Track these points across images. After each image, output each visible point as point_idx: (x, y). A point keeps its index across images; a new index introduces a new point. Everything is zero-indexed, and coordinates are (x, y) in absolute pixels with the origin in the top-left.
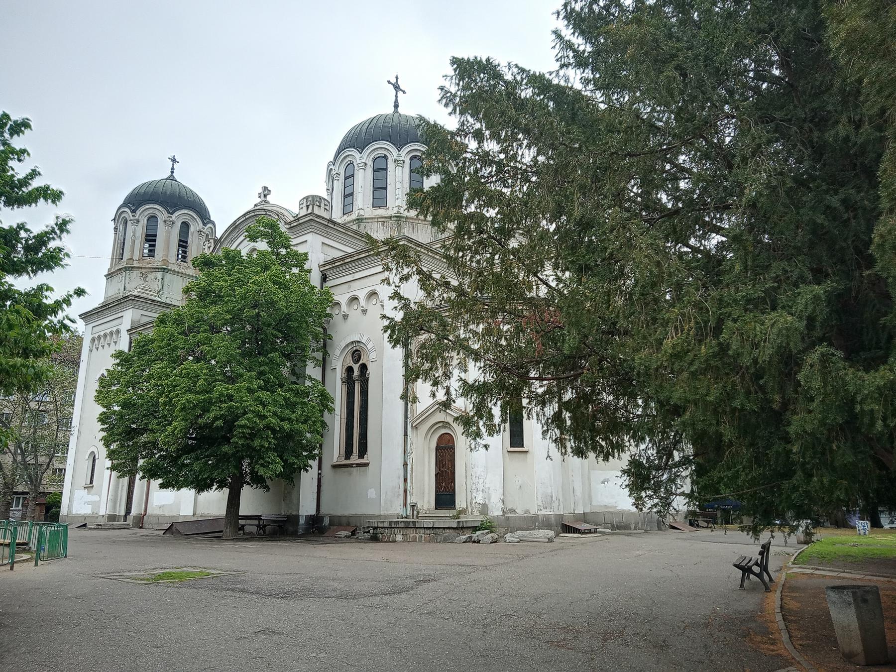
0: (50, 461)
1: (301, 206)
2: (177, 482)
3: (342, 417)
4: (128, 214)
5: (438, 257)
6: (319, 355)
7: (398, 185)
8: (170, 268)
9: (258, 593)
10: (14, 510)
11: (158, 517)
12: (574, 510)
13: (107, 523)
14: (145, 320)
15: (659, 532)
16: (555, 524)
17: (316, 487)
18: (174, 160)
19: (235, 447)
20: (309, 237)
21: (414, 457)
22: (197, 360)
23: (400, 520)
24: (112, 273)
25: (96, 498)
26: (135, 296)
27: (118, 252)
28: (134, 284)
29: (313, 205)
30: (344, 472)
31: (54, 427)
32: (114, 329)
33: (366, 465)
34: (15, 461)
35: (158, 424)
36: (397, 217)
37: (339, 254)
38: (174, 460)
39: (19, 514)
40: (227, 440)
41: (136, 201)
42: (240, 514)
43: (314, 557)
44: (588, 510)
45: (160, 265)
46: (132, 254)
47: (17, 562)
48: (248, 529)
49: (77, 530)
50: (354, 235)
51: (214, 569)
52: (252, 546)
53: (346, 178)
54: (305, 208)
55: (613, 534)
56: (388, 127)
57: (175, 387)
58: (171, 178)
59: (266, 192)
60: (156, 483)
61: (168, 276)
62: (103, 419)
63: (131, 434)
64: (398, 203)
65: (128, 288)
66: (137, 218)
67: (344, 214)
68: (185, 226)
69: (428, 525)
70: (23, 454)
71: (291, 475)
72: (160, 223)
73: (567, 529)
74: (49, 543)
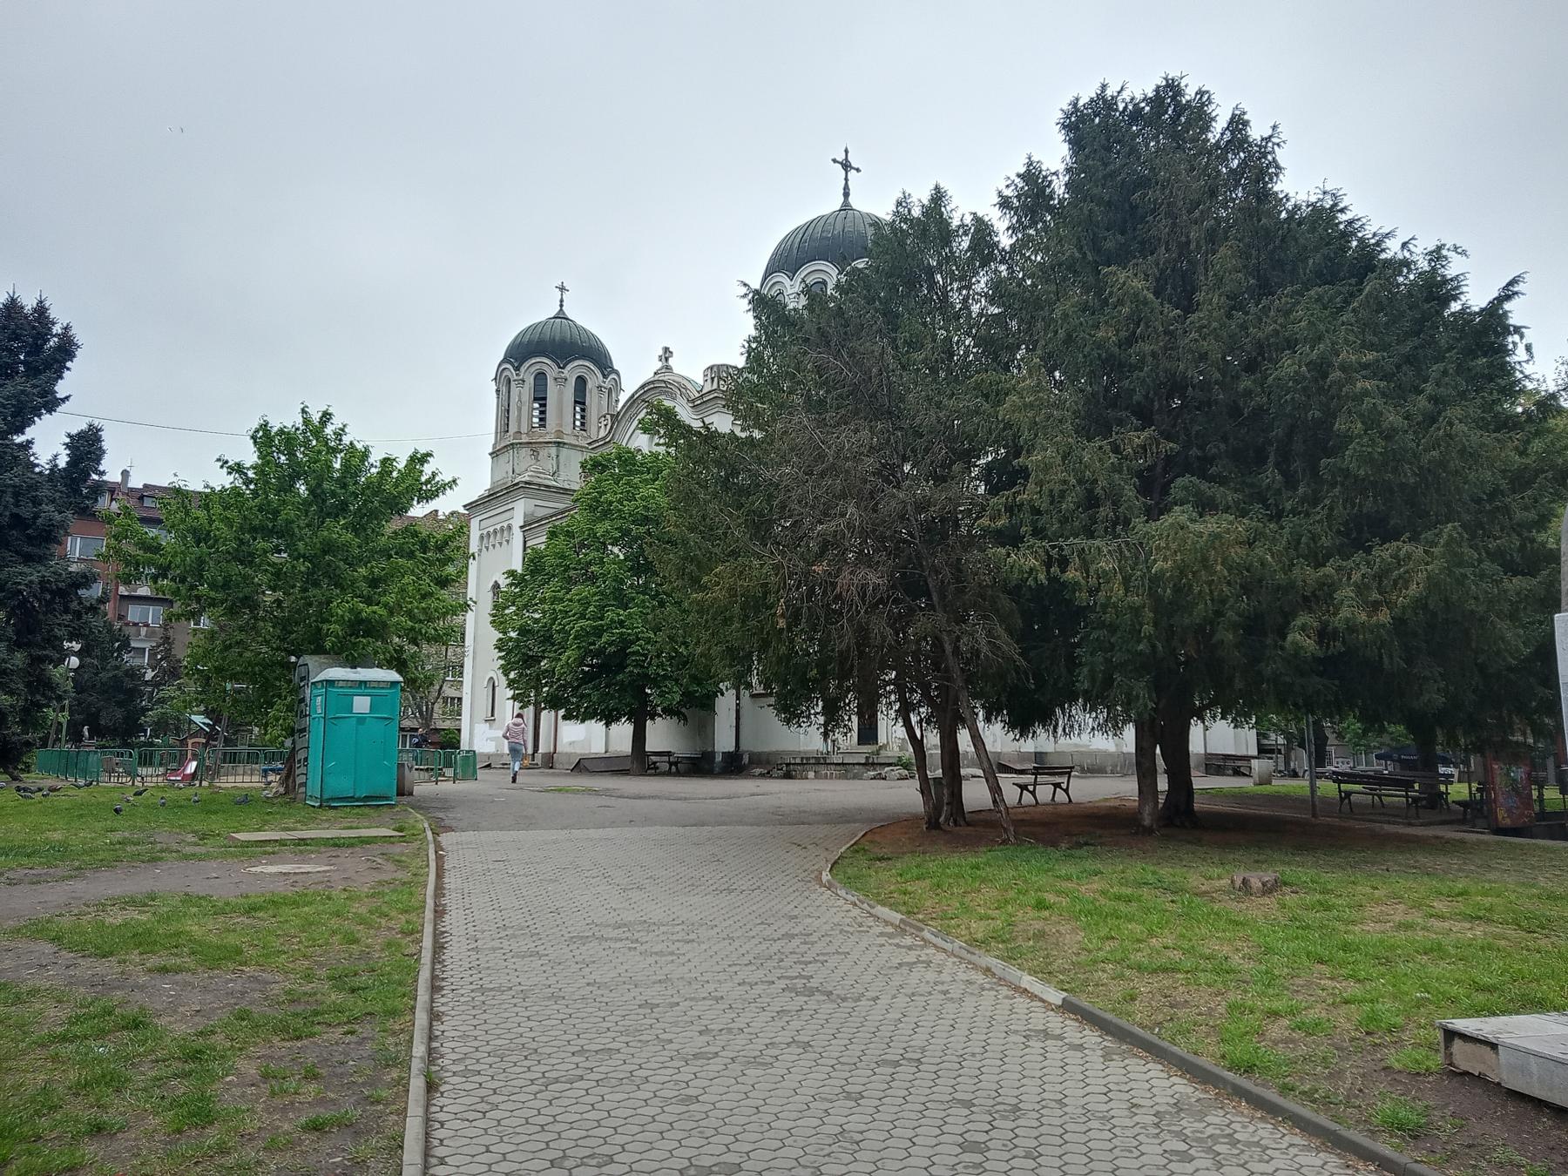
4: (512, 373)
8: (565, 441)
11: (569, 755)
14: (541, 513)
18: (562, 289)
26: (526, 483)
28: (525, 467)
32: (505, 525)
41: (520, 352)
46: (519, 426)
54: (709, 381)
56: (828, 238)
58: (560, 315)
61: (564, 452)
63: (530, 661)
65: (517, 471)
68: (581, 381)
72: (550, 381)
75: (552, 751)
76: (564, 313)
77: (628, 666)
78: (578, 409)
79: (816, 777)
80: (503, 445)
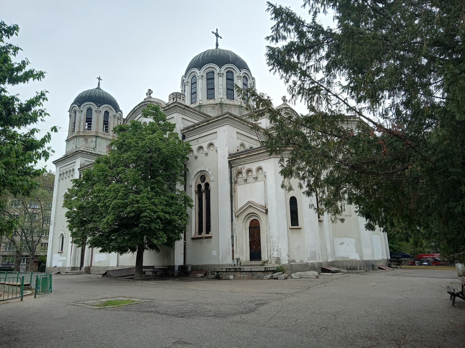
0: (40, 239)
1: (170, 99)
3: (196, 212)
4: (77, 108)
5: (246, 124)
7: (220, 87)
10: (22, 265)
11: (98, 267)
12: (327, 260)
13: (71, 271)
14: (87, 163)
15: (374, 271)
16: (317, 268)
17: (183, 250)
18: (99, 79)
20: (175, 115)
22: (118, 182)
23: (230, 267)
24: (69, 139)
25: (65, 258)
26: (82, 151)
27: (72, 128)
28: (81, 144)
30: (198, 242)
31: (41, 221)
32: (71, 169)
33: (210, 237)
34: (21, 239)
35: (98, 217)
36: (220, 104)
37: (191, 124)
38: (108, 237)
39: (25, 267)
40: (137, 226)
42: (144, 265)
43: (190, 289)
44: (334, 260)
46: (79, 129)
47: (25, 296)
48: (147, 273)
49: (55, 275)
50: (199, 114)
51: (136, 298)
54: (172, 99)
55: (349, 273)
56: (214, 56)
57: (107, 197)
58: (98, 88)
59: (150, 92)
60: (97, 250)
61: (99, 140)
62: (68, 215)
63: (83, 223)
64: (221, 96)
65: (78, 147)
66: (81, 109)
67: (191, 104)
68: (107, 113)
69: (248, 270)
71: (170, 244)
72: (94, 112)
73: (324, 270)
76: (100, 88)
77: (141, 223)
79: (234, 279)
80: (72, 136)
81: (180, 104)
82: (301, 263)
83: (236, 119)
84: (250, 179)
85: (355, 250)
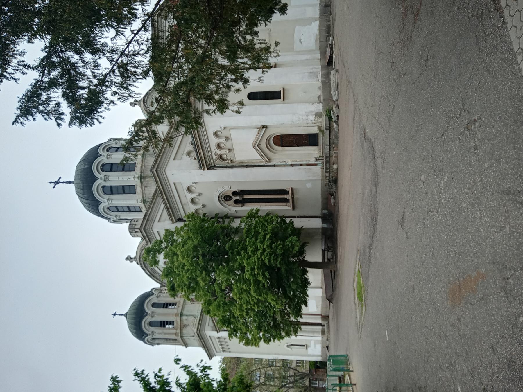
2: (303, 297)
4: (149, 338)
6: (227, 221)
9: (372, 238)
11: (323, 308)
12: (318, 59)
14: (211, 324)
18: (115, 315)
19: (282, 265)
20: (155, 230)
21: (288, 161)
22: (231, 290)
28: (191, 331)
29: (135, 229)
31: (273, 368)
32: (217, 340)
33: (292, 189)
34: (292, 387)
36: (141, 179)
37: (165, 212)
39: (321, 382)
40: (279, 269)
44: (319, 52)
45: (178, 318)
47: (351, 382)
48: (330, 257)
51: (355, 269)
52: (340, 252)
53: (118, 211)
54: (137, 234)
55: (333, 35)
56: (83, 186)
58: (126, 315)
59: (129, 258)
60: (304, 308)
61: (185, 312)
63: (276, 326)
64: (132, 179)
65: (193, 335)
68: (154, 305)
70: (289, 384)
73: (330, 62)
74: (339, 365)
75: (320, 316)
78: (170, 307)
79: (337, 163)
81: (142, 225)
82: (321, 88)
83: (158, 161)
84: (228, 145)
85: (309, 26)
